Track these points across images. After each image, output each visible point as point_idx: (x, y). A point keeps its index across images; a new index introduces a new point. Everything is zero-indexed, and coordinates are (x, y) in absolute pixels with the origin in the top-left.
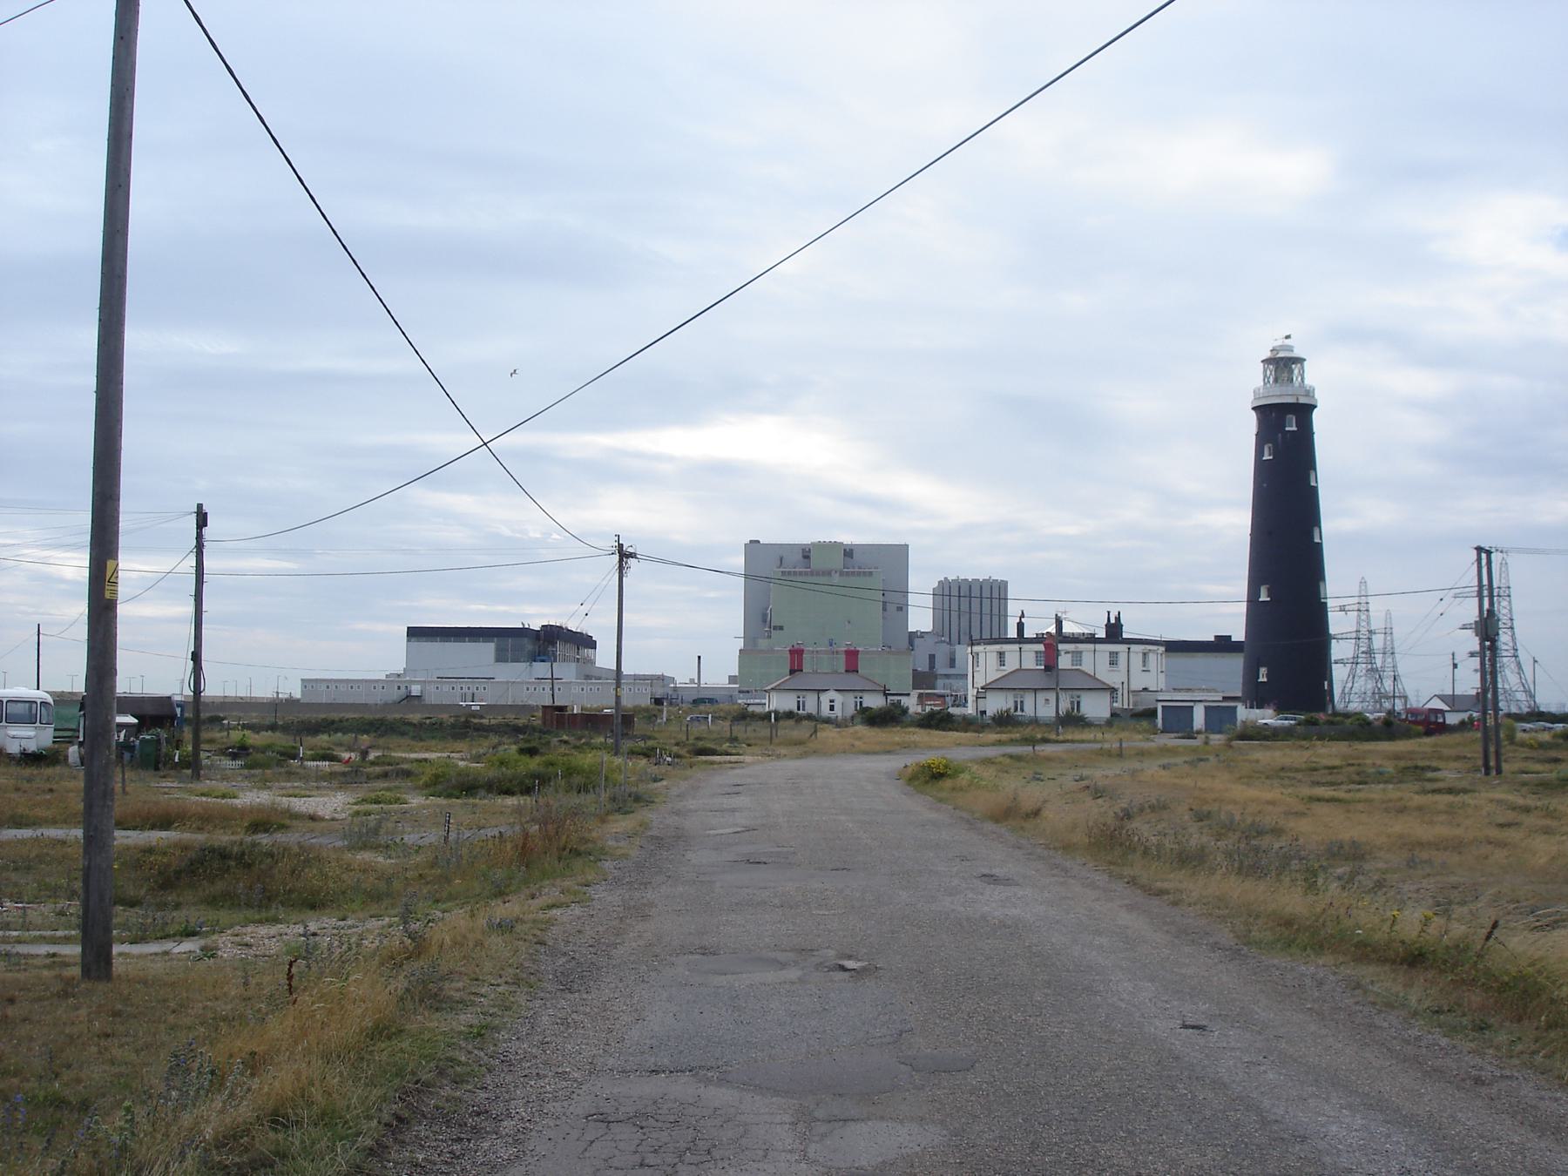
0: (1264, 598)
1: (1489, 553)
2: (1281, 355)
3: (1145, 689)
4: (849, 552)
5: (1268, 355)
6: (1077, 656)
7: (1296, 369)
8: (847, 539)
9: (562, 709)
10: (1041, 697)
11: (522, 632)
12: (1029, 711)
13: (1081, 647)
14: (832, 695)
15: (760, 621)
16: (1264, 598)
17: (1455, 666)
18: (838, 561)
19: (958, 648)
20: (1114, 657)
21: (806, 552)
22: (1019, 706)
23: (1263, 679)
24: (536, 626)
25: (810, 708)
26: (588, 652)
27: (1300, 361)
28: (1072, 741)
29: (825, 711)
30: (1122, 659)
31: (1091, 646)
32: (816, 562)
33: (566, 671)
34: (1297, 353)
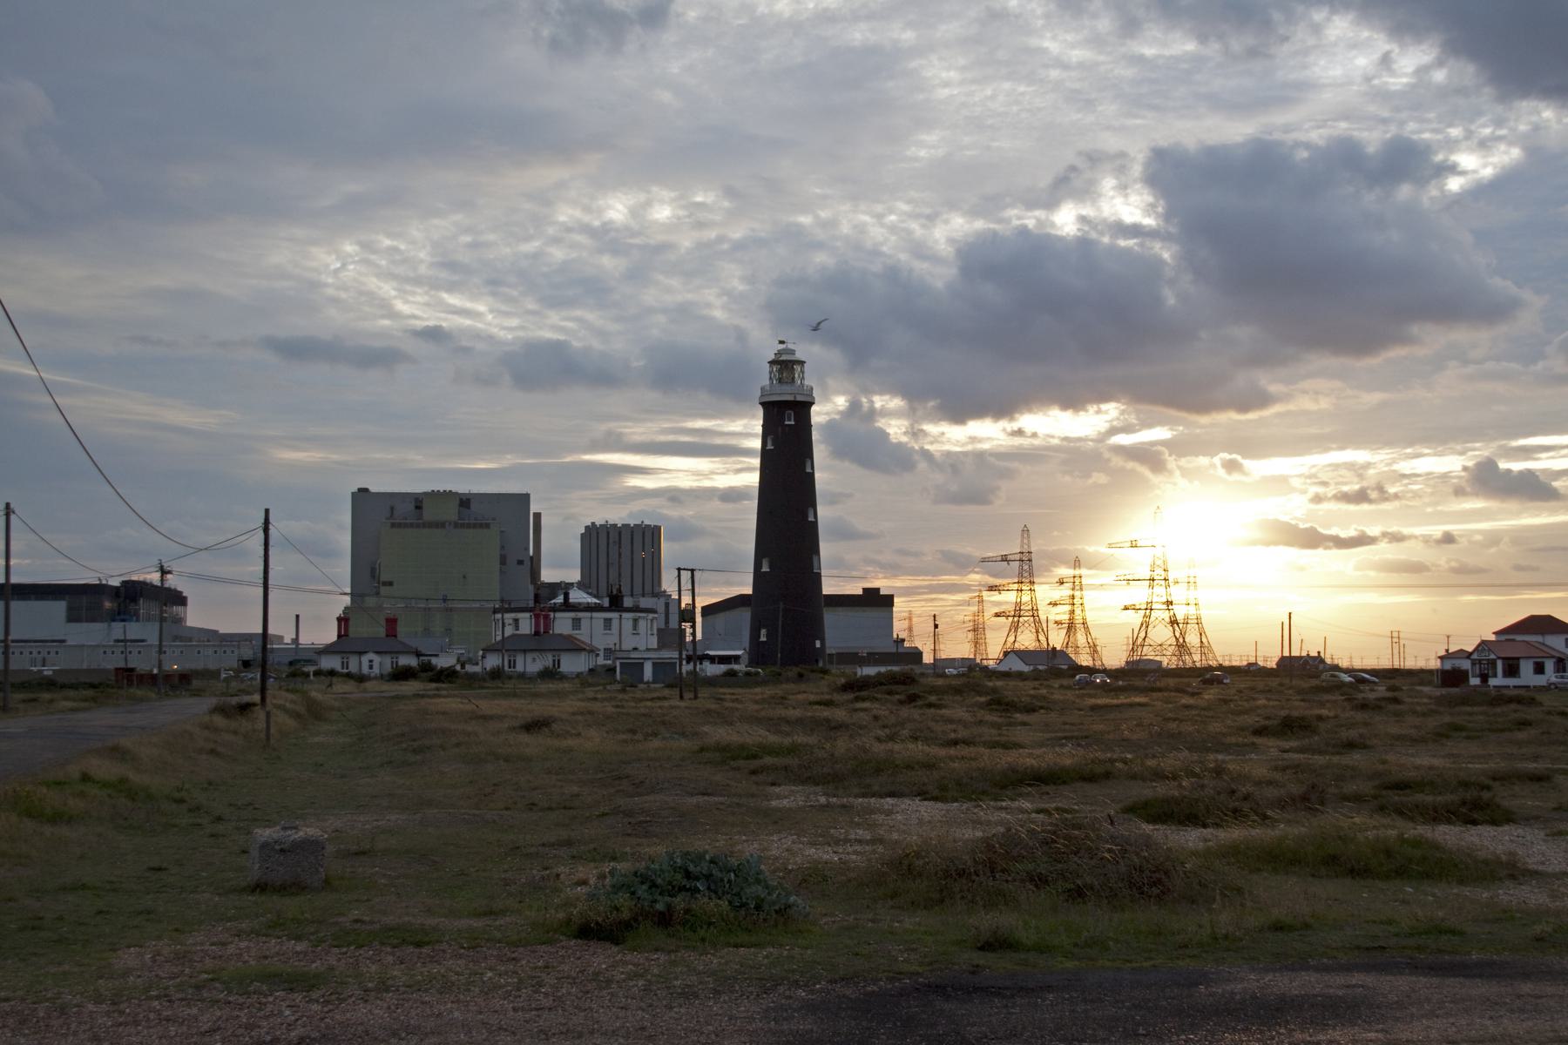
0: (765, 569)
1: (692, 571)
2: (784, 358)
3: (635, 649)
4: (465, 501)
5: (772, 357)
6: (576, 623)
7: (797, 368)
8: (462, 488)
9: (132, 670)
10: (529, 657)
11: (97, 590)
12: (519, 668)
13: (580, 615)
14: (371, 656)
15: (368, 575)
16: (765, 569)
17: (936, 626)
18: (451, 513)
20: (608, 622)
21: (418, 502)
22: (512, 664)
23: (763, 639)
24: (115, 582)
25: (353, 667)
26: (177, 609)
27: (802, 363)
28: (652, 699)
29: (365, 670)
30: (615, 624)
31: (588, 614)
32: (429, 514)
33: (142, 630)
34: (799, 356)
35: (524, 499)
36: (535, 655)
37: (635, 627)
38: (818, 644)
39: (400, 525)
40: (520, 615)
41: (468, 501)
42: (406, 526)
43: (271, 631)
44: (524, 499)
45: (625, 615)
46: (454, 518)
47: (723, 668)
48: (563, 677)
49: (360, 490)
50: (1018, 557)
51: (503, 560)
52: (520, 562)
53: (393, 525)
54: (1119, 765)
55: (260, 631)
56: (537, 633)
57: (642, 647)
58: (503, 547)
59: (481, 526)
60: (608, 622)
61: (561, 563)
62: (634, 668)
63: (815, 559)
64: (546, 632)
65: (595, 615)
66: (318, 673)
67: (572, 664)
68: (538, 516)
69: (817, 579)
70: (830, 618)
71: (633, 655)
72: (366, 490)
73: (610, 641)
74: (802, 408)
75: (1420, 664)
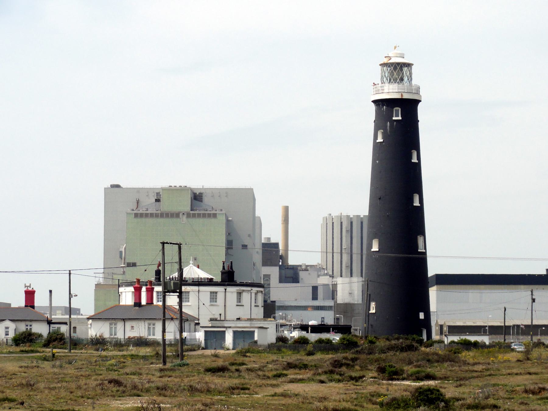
10: (128, 324)
12: (120, 335)
17: (534, 300)
18: (185, 205)
19: (339, 281)
20: (214, 296)
23: (373, 311)
27: (409, 65)
31: (196, 288)
35: (105, 188)
36: (134, 323)
37: (239, 299)
38: (422, 316)
39: (141, 215)
41: (201, 195)
42: (147, 215)
44: (105, 188)
46: (188, 208)
49: (113, 186)
53: (136, 215)
54: (154, 361)
56: (138, 304)
59: (209, 216)
60: (214, 296)
63: (420, 240)
65: (202, 288)
66: (249, 370)
72: (118, 186)
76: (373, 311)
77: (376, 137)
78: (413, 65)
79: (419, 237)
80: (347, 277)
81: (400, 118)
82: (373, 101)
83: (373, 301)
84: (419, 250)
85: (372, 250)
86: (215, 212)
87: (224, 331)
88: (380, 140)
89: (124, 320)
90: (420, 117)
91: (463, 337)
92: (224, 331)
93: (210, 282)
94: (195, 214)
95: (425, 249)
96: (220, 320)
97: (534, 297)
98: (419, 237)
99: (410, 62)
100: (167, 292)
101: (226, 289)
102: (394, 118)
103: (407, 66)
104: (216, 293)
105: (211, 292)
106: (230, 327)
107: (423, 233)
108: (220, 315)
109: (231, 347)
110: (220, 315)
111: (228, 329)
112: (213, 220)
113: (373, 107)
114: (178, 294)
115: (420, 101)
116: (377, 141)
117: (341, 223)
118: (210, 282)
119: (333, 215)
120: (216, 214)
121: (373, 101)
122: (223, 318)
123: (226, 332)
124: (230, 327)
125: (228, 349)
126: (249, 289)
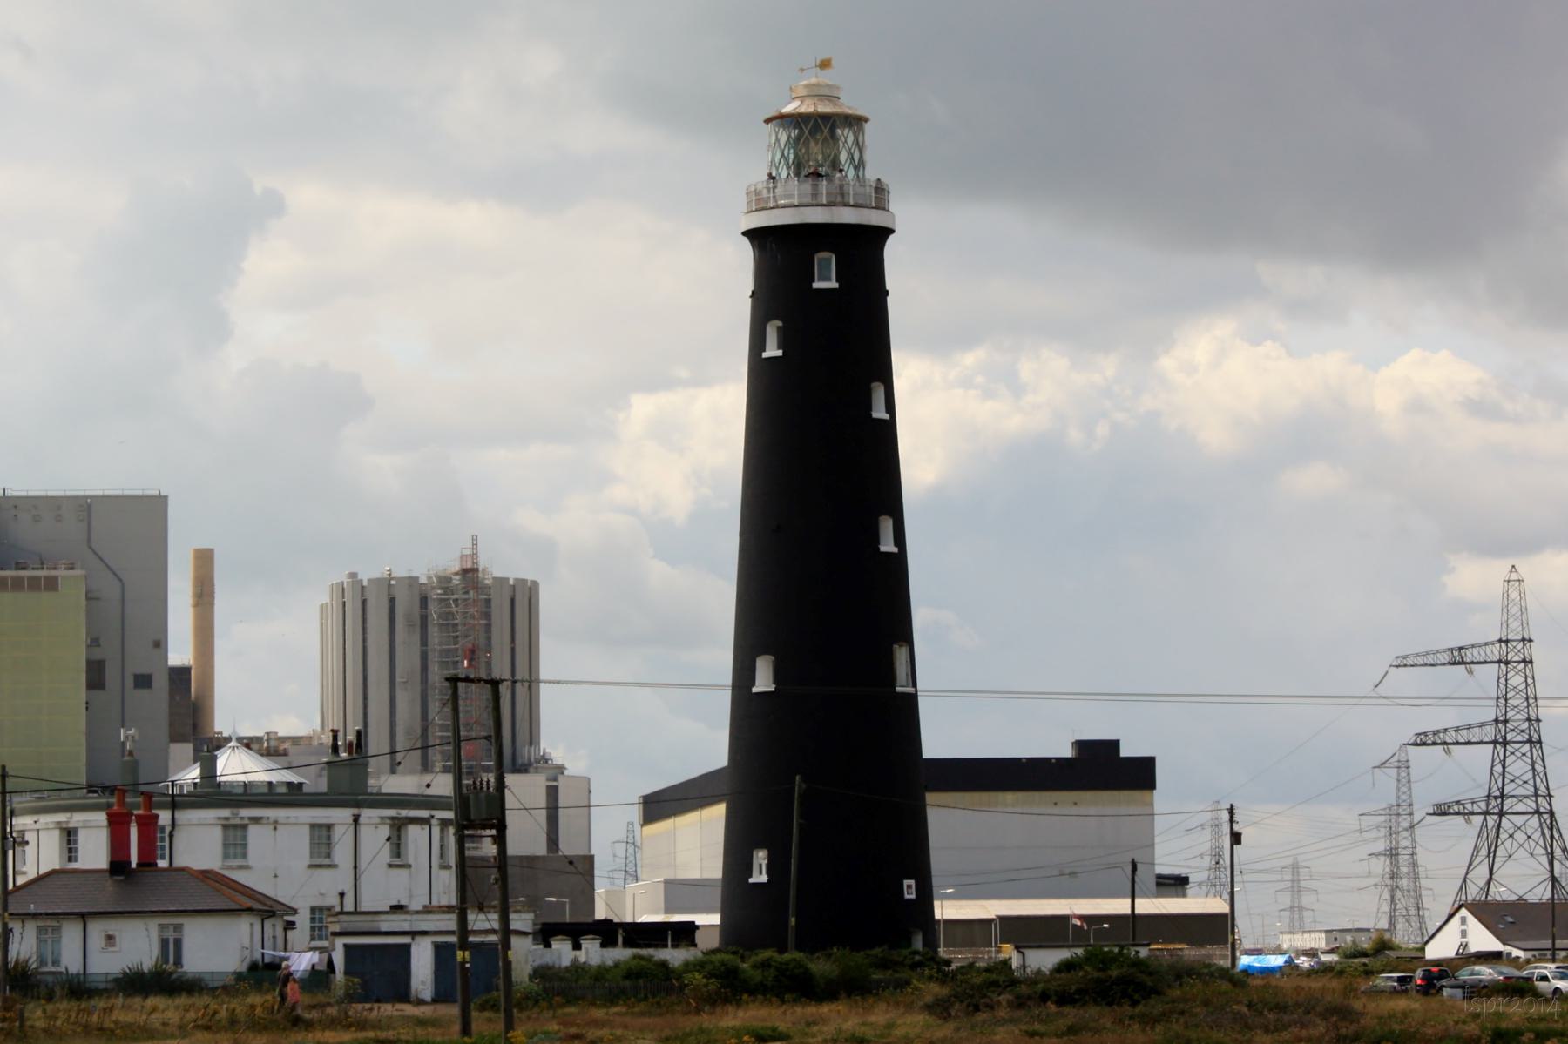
3: (398, 908)
7: (846, 135)
10: (97, 929)
12: (70, 961)
17: (1236, 838)
27: (855, 122)
34: (849, 104)
36: (112, 926)
40: (77, 819)
43: (970, 687)
45: (368, 814)
47: (620, 954)
48: (192, 986)
50: (1495, 652)
51: (96, 676)
52: (143, 681)
55: (1137, 901)
56: (118, 866)
57: (416, 905)
58: (94, 642)
60: (322, 836)
61: (271, 680)
62: (379, 970)
63: (901, 654)
64: (147, 862)
67: (215, 949)
68: (204, 561)
69: (906, 710)
70: (949, 823)
71: (386, 924)
73: (327, 887)
74: (862, 248)
75: (695, 874)
76: (760, 877)
77: (758, 342)
78: (866, 120)
79: (896, 646)
80: (412, 772)
81: (834, 285)
82: (745, 234)
83: (760, 846)
84: (898, 689)
85: (754, 690)
86: (53, 573)
87: (408, 946)
88: (772, 351)
89: (83, 917)
90: (891, 282)
91: (644, 952)
92: (408, 946)
93: (293, 797)
94: (21, 579)
95: (915, 685)
96: (342, 913)
97: (1236, 828)
98: (896, 646)
99: (860, 112)
100: (467, 828)
101: (356, 819)
102: (816, 285)
103: (850, 126)
104: (329, 827)
105: (313, 826)
106: (424, 933)
107: (908, 639)
108: (342, 895)
109: (427, 994)
110: (342, 895)
111: (418, 939)
112: (46, 597)
113: (745, 255)
114: (494, 832)
115: (891, 231)
116: (765, 355)
117: (392, 601)
118: (293, 797)
119: (365, 577)
120: (56, 578)
121: (745, 234)
122: (349, 907)
123: (413, 950)
124: (424, 933)
125: (421, 1002)
126: (424, 813)
